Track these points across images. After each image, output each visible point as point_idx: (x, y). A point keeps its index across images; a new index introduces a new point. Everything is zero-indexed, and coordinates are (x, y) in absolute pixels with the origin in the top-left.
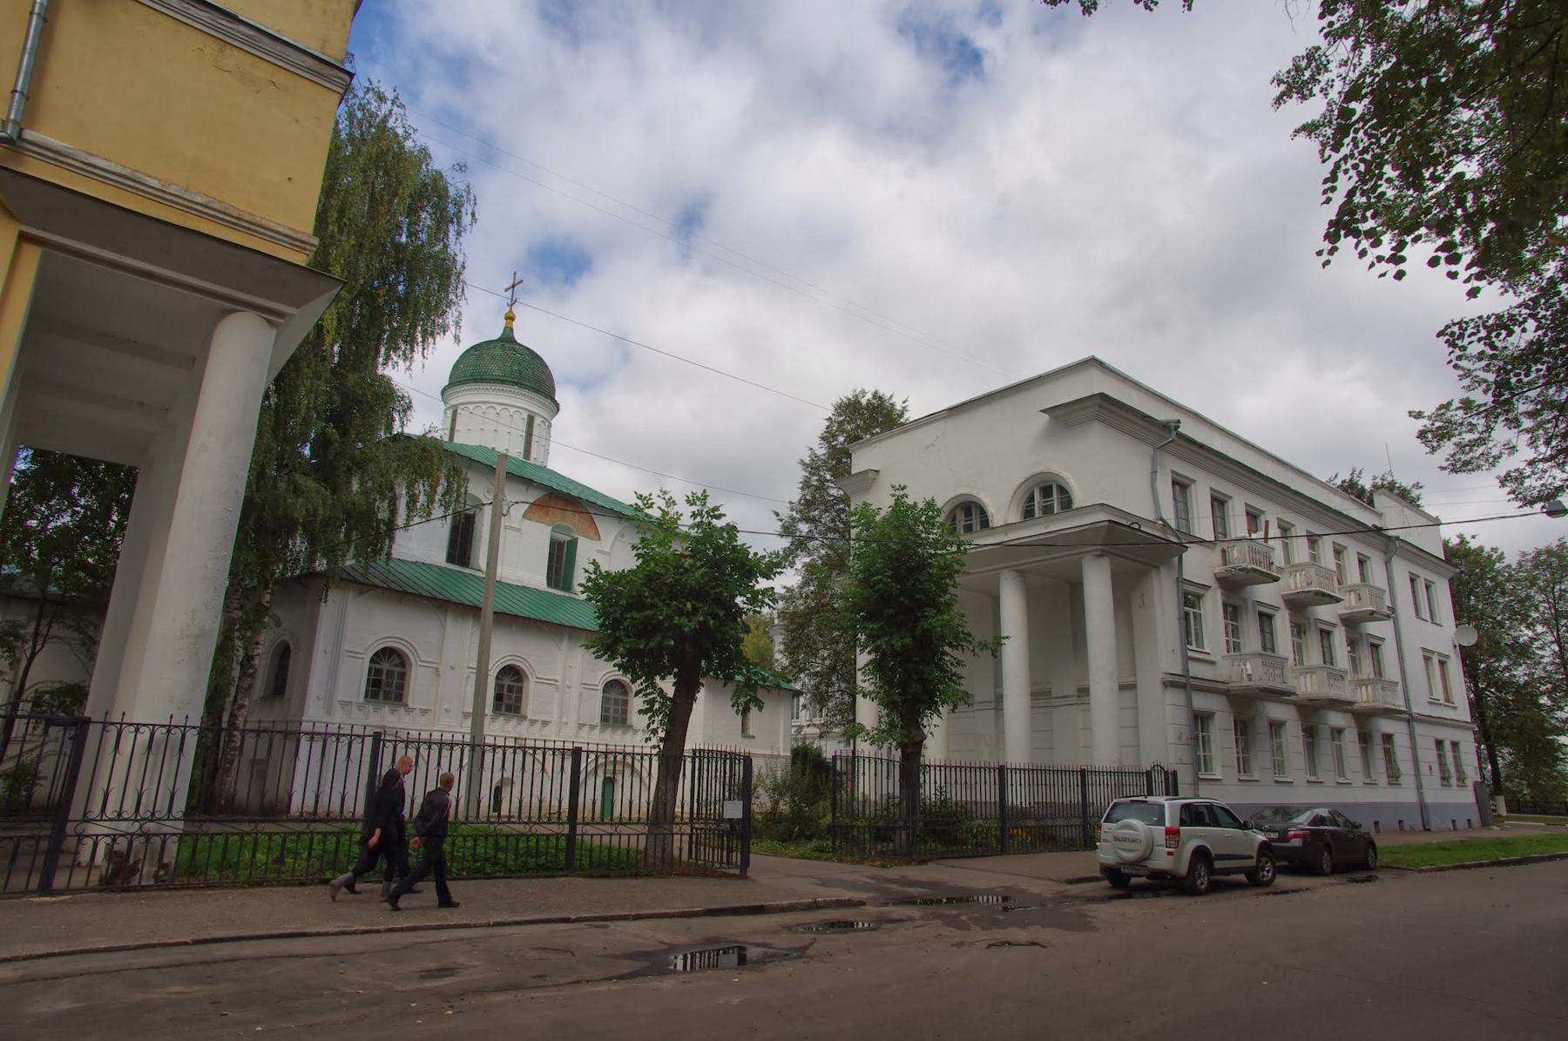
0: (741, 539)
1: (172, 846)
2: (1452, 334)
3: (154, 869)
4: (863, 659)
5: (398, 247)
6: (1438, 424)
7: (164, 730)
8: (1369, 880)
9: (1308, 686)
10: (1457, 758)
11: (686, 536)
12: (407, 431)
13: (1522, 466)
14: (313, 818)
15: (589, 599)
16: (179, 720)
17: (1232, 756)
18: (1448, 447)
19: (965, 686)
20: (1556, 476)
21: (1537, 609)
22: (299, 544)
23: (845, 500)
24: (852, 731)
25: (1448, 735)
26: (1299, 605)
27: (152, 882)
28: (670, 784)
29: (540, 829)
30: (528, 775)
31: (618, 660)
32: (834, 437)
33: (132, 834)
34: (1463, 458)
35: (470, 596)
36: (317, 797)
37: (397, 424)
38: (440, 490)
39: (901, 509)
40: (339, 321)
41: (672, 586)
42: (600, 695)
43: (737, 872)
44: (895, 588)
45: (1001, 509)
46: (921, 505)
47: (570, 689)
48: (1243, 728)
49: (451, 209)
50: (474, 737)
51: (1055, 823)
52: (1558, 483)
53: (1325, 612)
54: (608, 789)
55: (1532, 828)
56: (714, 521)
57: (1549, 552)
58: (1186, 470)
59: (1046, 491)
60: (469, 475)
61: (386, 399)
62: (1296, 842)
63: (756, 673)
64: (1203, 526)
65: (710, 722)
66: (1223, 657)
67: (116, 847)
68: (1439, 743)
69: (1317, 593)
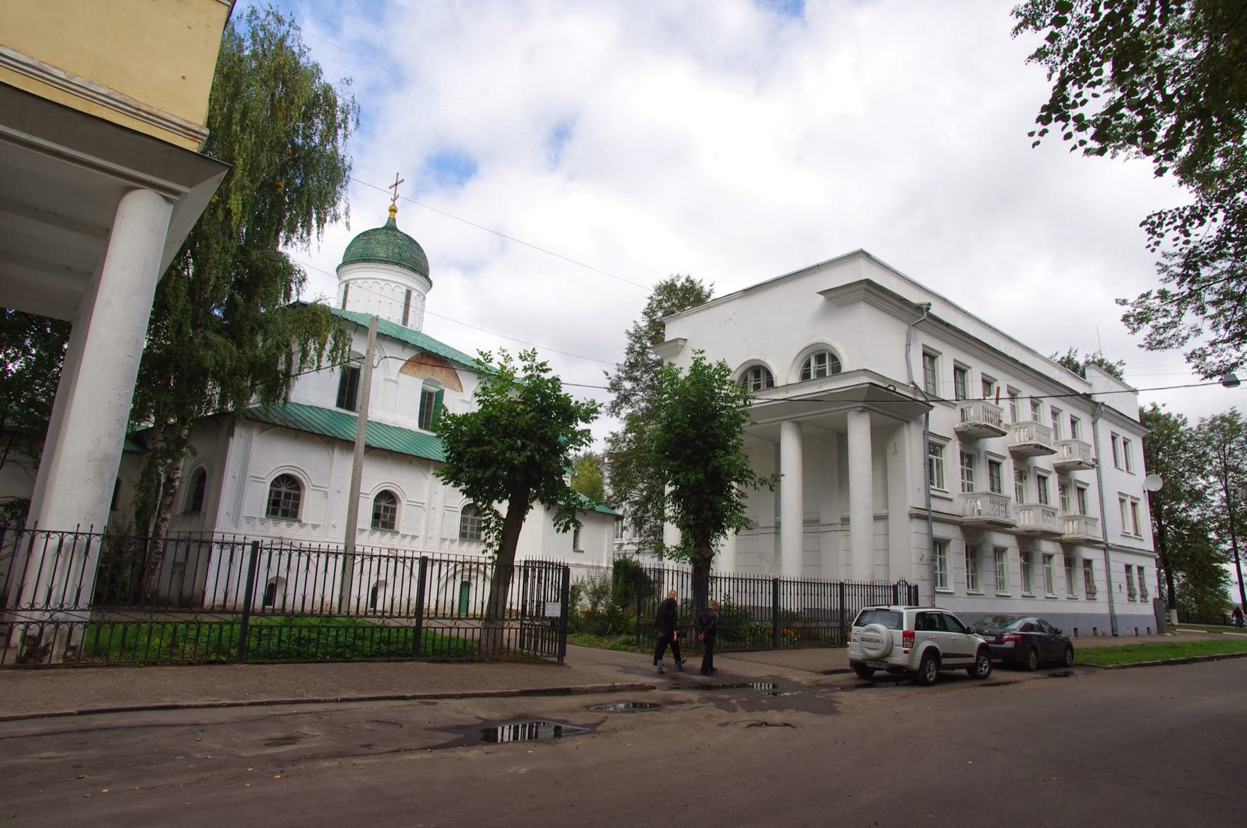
0: (564, 390)
1: (78, 632)
2: (1152, 223)
3: (63, 651)
4: (668, 489)
5: (296, 148)
6: (1139, 310)
7: (72, 537)
8: (1066, 675)
9: (1026, 521)
10: (1141, 580)
11: (518, 386)
12: (303, 299)
13: (1205, 345)
14: (223, 609)
15: (439, 437)
16: (84, 528)
17: (963, 574)
18: (1146, 329)
19: (747, 514)
20: (1231, 355)
21: (1211, 464)
22: (213, 390)
23: (659, 363)
24: (659, 550)
25: (1135, 561)
26: (1021, 456)
27: (61, 661)
28: (501, 588)
29: (392, 623)
30: (399, 579)
31: (463, 486)
32: (654, 312)
33: (43, 622)
34: (1158, 338)
35: (350, 433)
36: (226, 595)
37: (294, 292)
38: (328, 347)
39: (698, 369)
40: (243, 204)
41: (506, 427)
42: (459, 515)
43: (556, 659)
44: (692, 432)
45: (784, 372)
46: (714, 366)
47: (434, 513)
48: (973, 553)
49: (340, 116)
51: (820, 627)
52: (1233, 360)
53: (1042, 462)
54: (465, 590)
55: (1197, 635)
56: (542, 375)
57: (1223, 418)
58: (935, 344)
59: (821, 358)
60: (353, 336)
61: (285, 274)
62: (1010, 644)
63: (574, 499)
64: (946, 389)
65: (538, 536)
66: (960, 497)
67: (29, 633)
68: (1128, 568)
69: (1037, 446)
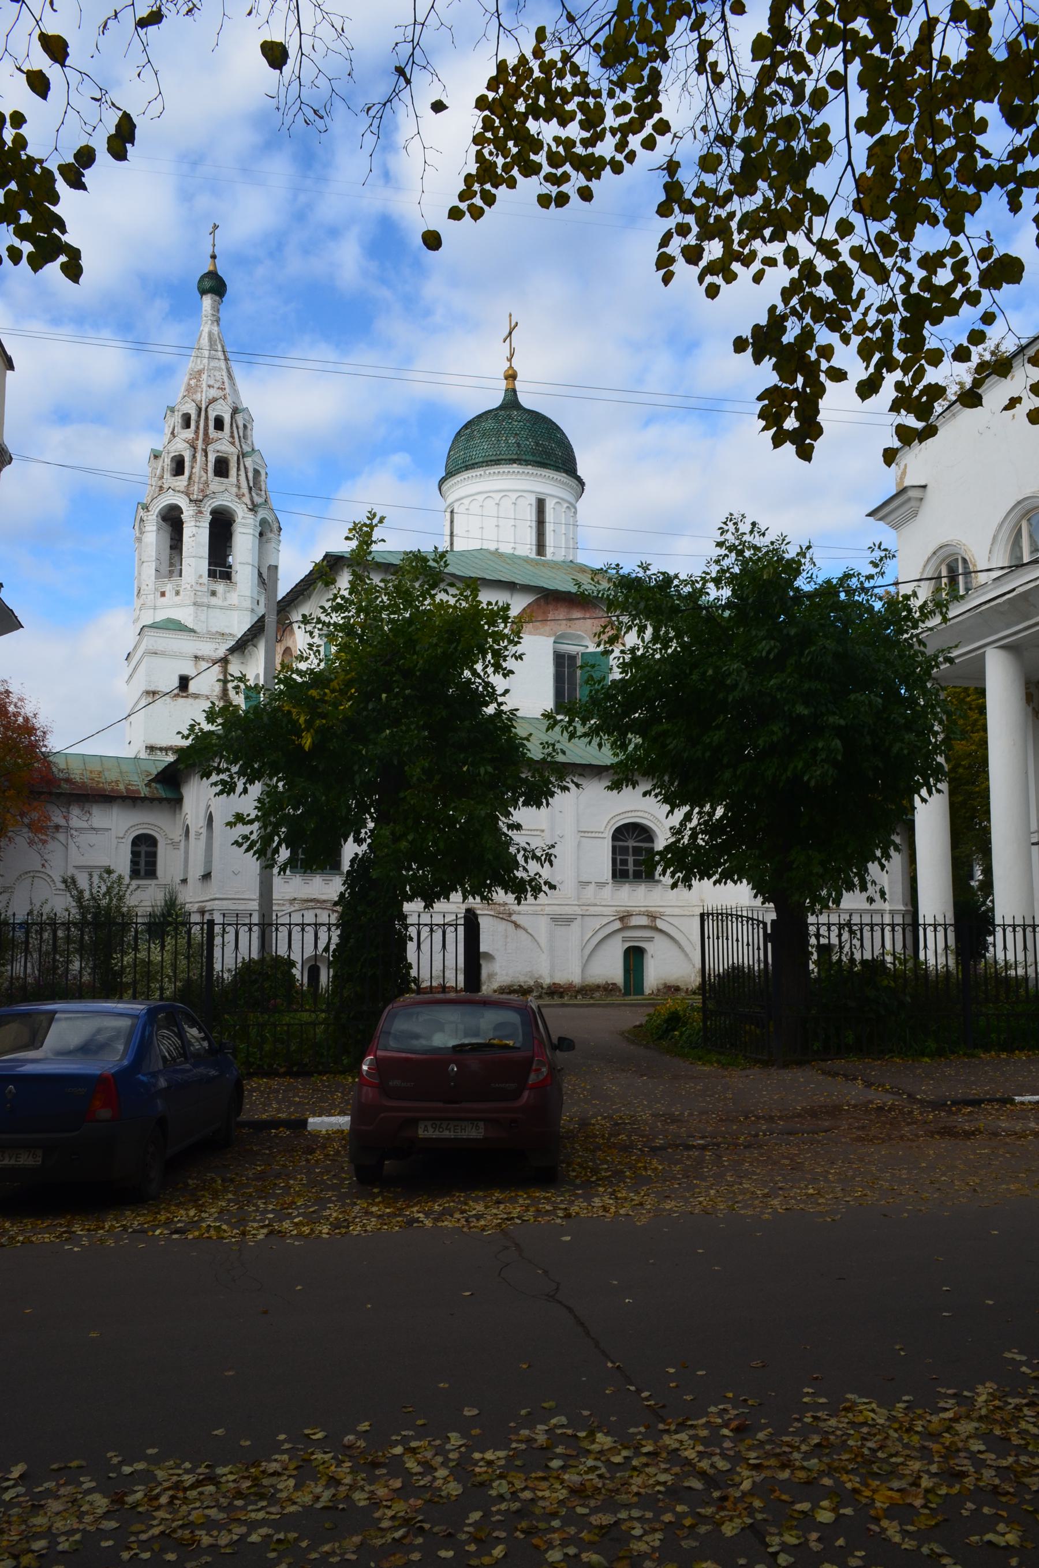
50: (263, 916)
